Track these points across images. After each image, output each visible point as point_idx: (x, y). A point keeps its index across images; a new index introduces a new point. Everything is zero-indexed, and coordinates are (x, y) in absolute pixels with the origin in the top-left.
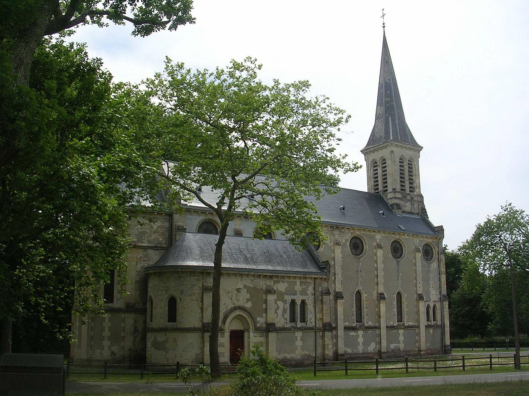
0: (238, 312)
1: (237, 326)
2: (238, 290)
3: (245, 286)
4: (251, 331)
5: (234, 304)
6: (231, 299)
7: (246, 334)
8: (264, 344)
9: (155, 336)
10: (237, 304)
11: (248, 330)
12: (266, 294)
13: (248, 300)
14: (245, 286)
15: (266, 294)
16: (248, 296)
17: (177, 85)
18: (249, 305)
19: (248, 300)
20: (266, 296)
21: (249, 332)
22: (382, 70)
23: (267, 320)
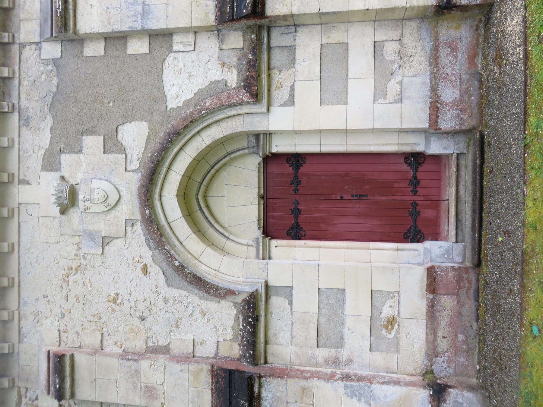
0: (171, 208)
1: (240, 198)
2: (69, 200)
3: (51, 163)
4: (259, 125)
5: (129, 223)
6: (106, 241)
7: (279, 146)
8: (336, 36)
9: (253, 246)
10: (130, 207)
11: (259, 138)
12: (79, 40)
13: (112, 145)
14: (51, 163)
15: (79, 40)
16: (93, 143)
17: (169, 135)
18: (136, 136)
19: (112, 145)
20: (93, 37)
21: (268, 135)
22: (342, 168)
23: (207, 29)
